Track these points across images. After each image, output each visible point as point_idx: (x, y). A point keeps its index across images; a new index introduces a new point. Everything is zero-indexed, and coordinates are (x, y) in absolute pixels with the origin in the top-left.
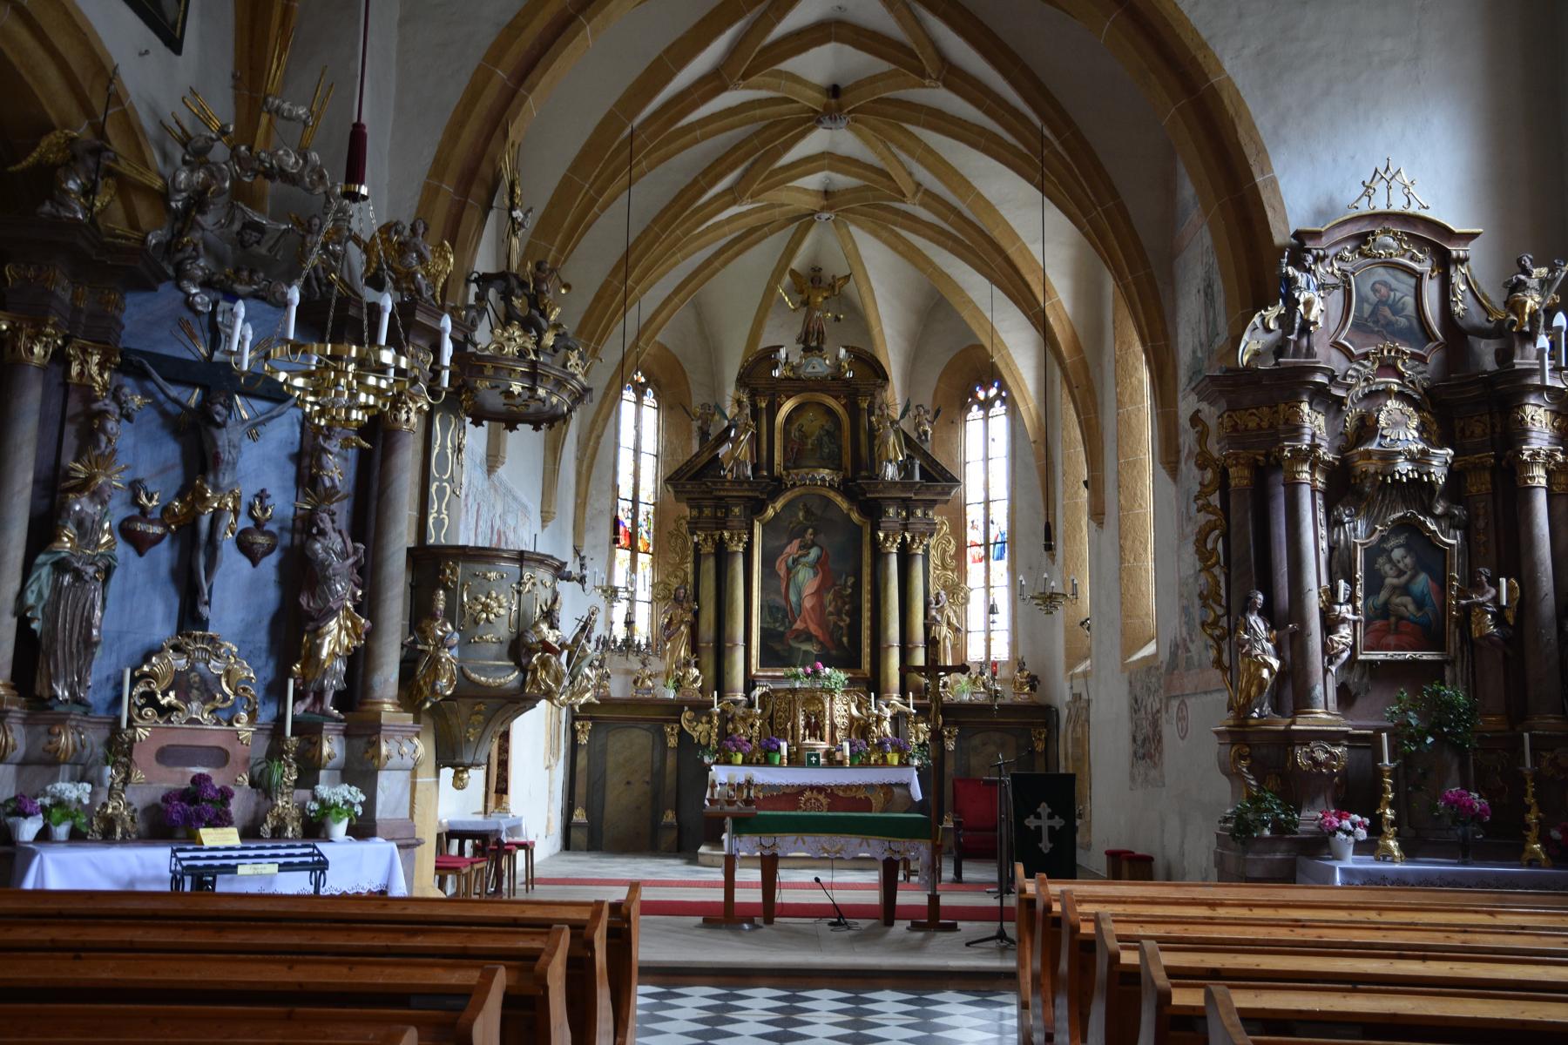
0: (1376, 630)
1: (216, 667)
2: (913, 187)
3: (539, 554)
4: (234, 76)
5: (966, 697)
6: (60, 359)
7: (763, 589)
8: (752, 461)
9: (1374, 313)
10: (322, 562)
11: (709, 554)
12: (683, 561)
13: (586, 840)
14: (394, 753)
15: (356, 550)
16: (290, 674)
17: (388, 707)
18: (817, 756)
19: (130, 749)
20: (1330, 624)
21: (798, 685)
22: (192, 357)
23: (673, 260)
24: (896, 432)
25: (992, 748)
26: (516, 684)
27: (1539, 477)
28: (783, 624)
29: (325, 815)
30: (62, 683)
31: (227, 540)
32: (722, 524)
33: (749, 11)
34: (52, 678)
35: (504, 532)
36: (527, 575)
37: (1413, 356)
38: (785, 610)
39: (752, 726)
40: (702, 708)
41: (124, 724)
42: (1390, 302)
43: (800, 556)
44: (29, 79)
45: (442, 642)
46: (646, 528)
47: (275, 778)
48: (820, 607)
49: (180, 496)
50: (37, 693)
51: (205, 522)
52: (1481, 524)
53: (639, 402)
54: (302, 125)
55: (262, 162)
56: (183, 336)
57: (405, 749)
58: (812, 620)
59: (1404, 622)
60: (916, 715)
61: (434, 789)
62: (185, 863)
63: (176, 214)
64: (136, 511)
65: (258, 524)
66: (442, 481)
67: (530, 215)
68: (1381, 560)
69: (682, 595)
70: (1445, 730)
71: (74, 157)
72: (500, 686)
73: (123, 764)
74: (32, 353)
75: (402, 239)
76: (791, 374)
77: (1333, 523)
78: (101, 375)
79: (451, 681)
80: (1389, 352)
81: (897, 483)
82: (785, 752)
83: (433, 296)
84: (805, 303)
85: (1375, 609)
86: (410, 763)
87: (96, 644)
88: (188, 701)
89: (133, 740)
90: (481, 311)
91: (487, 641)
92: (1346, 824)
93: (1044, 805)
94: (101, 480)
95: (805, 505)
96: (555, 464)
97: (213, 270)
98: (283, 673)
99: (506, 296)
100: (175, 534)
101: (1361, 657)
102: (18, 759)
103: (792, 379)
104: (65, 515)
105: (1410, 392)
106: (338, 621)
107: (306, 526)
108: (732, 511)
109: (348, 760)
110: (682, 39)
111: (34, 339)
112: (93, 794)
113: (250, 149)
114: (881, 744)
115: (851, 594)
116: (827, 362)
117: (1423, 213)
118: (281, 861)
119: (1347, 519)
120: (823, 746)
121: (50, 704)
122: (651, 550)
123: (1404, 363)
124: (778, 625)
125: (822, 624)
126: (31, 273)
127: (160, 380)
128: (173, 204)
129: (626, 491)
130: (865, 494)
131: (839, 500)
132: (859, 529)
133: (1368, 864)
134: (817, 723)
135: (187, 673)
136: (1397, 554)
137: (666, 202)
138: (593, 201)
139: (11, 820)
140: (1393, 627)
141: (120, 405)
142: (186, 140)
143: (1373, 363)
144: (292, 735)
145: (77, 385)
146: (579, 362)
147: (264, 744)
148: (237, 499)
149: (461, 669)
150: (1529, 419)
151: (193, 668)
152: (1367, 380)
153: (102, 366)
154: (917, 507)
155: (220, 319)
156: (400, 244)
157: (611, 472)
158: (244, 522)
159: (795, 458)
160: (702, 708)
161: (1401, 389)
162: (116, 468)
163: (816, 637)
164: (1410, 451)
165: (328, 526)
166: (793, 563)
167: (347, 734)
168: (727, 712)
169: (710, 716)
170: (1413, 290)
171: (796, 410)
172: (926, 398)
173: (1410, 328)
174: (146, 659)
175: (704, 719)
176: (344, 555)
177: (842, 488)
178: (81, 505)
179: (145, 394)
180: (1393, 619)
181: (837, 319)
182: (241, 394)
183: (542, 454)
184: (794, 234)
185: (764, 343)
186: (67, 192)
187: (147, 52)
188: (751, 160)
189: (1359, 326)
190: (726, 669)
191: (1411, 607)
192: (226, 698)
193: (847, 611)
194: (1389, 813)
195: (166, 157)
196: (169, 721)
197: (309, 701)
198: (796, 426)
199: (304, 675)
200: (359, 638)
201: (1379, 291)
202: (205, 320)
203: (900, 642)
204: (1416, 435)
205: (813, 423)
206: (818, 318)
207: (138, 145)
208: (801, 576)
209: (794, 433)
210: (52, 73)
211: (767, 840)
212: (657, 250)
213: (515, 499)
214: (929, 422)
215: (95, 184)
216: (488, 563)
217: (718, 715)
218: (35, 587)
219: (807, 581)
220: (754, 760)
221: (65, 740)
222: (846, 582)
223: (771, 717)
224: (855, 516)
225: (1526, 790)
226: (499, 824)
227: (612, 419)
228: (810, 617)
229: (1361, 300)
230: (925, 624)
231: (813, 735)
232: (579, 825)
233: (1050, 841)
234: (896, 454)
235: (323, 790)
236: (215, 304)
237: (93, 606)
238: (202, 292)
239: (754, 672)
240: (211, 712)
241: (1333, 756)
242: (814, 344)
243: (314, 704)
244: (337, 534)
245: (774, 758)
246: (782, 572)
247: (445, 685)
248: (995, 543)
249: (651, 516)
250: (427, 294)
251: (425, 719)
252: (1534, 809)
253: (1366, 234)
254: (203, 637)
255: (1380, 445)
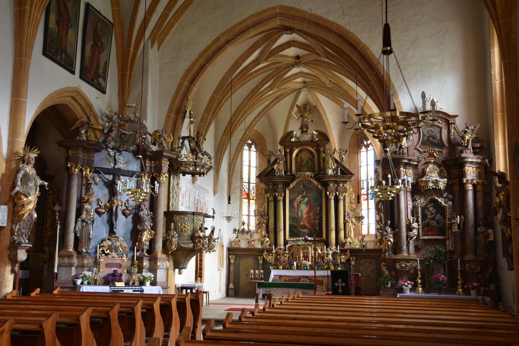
0: (426, 230)
1: (118, 244)
2: (329, 82)
3: (198, 212)
4: (118, 93)
5: (358, 247)
6: (81, 171)
7: (290, 211)
8: (284, 170)
9: (427, 139)
10: (142, 217)
11: (272, 200)
12: (264, 203)
13: (234, 293)
14: (161, 265)
15: (150, 214)
16: (135, 245)
17: (160, 253)
18: (307, 266)
19: (99, 263)
20: (409, 228)
21: (300, 243)
22: (110, 168)
23: (254, 108)
24: (332, 159)
25: (367, 264)
26: (192, 247)
27: (470, 187)
28: (296, 223)
29: (145, 280)
30: (84, 248)
31: (120, 213)
32: (275, 191)
33: (263, 45)
34: (82, 247)
35: (199, 200)
36: (195, 218)
37: (439, 151)
38: (297, 219)
39: (286, 257)
40: (269, 251)
41: (98, 258)
42: (432, 136)
43: (302, 201)
44: (74, 110)
45: (173, 237)
46: (253, 191)
47: (133, 271)
48: (309, 217)
49: (109, 202)
50: (79, 250)
51: (114, 208)
52: (456, 200)
53: (250, 150)
54: (134, 108)
55: (125, 118)
56: (108, 162)
57: (164, 264)
58: (306, 222)
59: (433, 228)
60: (340, 253)
61: (174, 275)
62: (112, 289)
63: (106, 134)
64: (99, 206)
65: (127, 208)
66: (173, 193)
67: (195, 119)
68: (426, 211)
69: (263, 214)
70: (437, 258)
71: (83, 125)
72: (188, 247)
73: (98, 267)
74: (75, 171)
75: (159, 134)
76: (297, 140)
77: (414, 200)
78: (90, 174)
79: (175, 246)
80: (431, 151)
81: (333, 176)
82: (295, 265)
83: (168, 148)
84: (302, 116)
85: (425, 224)
86: (165, 267)
87: (91, 239)
88: (112, 252)
89: (100, 262)
90: (182, 148)
91: (185, 236)
92: (406, 284)
93: (340, 279)
94: (91, 200)
95: (303, 184)
96: (217, 176)
97: (114, 145)
98: (134, 245)
99: (190, 142)
100: (107, 211)
101: (421, 238)
102: (76, 266)
103: (297, 142)
104: (83, 209)
105: (438, 162)
106: (147, 232)
107: (138, 208)
108: (278, 186)
109: (150, 267)
110: (243, 54)
111: (76, 168)
112: (92, 274)
113: (122, 115)
114: (328, 262)
115: (319, 213)
116: (309, 136)
117: (441, 110)
118: (133, 289)
119: (417, 199)
120: (309, 263)
121: (82, 253)
122: (255, 199)
123: (436, 154)
124: (294, 223)
125: (309, 223)
126: (75, 152)
127: (103, 174)
128: (105, 132)
129: (245, 179)
130: (322, 180)
131: (314, 181)
132: (321, 191)
133: (413, 294)
134: (307, 256)
135: (111, 245)
136: (431, 209)
137: (249, 93)
138: (221, 101)
139: (75, 280)
140: (430, 229)
141: (94, 181)
142: (107, 117)
143: (427, 154)
144: (136, 260)
145: (85, 177)
146: (208, 160)
147: (130, 262)
148: (122, 202)
149: (178, 243)
150: (466, 170)
151: (113, 244)
152: (425, 159)
153: (90, 172)
154: (341, 183)
155: (116, 157)
156: (159, 135)
157: (239, 175)
158: (124, 208)
159: (299, 168)
160: (269, 251)
161: (435, 161)
162: (94, 196)
163: (307, 227)
164: (432, 180)
165: (144, 208)
166: (299, 202)
167: (150, 260)
168: (278, 252)
169: (272, 253)
170: (439, 132)
171: (299, 152)
172: (346, 147)
173: (438, 143)
174: (102, 242)
175: (271, 255)
176: (148, 215)
177: (315, 178)
178: (87, 206)
179: (100, 177)
180: (430, 227)
181: (312, 121)
182: (122, 175)
183: (213, 173)
184: (296, 94)
185: (289, 130)
186: (82, 134)
187: (98, 98)
188: (274, 78)
189: (423, 143)
190: (278, 238)
191: (436, 224)
192: (121, 251)
193: (318, 218)
194: (419, 281)
195: (103, 120)
196: (108, 257)
197: (140, 252)
198: (299, 157)
199: (139, 246)
200: (152, 236)
201: (429, 133)
202: (113, 158)
203: (335, 229)
204: (437, 175)
205: (305, 156)
206: (306, 121)
207: (97, 119)
208: (302, 207)
209: (299, 160)
210: (79, 108)
211: (268, 290)
212: (247, 107)
213: (203, 189)
214: (344, 154)
215: (88, 131)
216: (185, 215)
217: (275, 253)
218: (78, 226)
219: (304, 208)
220: (286, 268)
221: (86, 262)
222: (317, 209)
223: (292, 254)
224: (320, 187)
225: (458, 275)
226: (195, 285)
227: (240, 157)
228: (305, 220)
229: (424, 135)
230: (344, 223)
231: (305, 259)
232: (231, 289)
233: (342, 290)
234: (332, 166)
235: (144, 274)
236: (115, 154)
237: (90, 230)
238: (112, 151)
239: (287, 239)
240: (117, 255)
241: (407, 266)
242: (305, 130)
243: (141, 253)
244: (146, 210)
245: (292, 267)
246: (296, 206)
247: (174, 248)
248: (371, 194)
249: (254, 188)
250: (166, 148)
251: (171, 257)
252: (460, 280)
253: (425, 117)
254: (115, 237)
255: (426, 178)
